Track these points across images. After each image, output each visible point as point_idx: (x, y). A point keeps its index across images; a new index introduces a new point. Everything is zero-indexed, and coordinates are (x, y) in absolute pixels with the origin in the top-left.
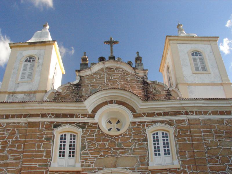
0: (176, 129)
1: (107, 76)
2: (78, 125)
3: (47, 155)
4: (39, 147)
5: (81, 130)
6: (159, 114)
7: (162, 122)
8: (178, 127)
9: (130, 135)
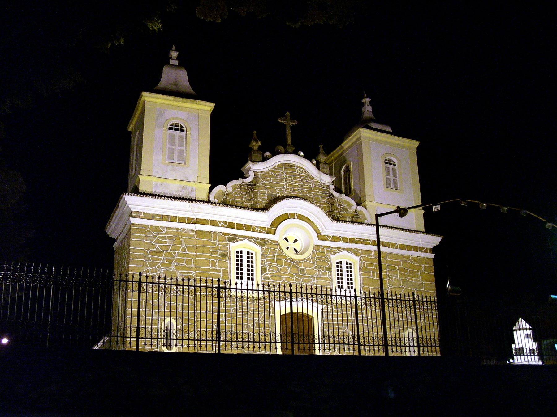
0: (361, 260)
1: (286, 177)
2: (256, 242)
3: (224, 275)
4: (213, 264)
5: (260, 248)
6: (345, 240)
7: (348, 250)
8: (364, 258)
9: (314, 261)
